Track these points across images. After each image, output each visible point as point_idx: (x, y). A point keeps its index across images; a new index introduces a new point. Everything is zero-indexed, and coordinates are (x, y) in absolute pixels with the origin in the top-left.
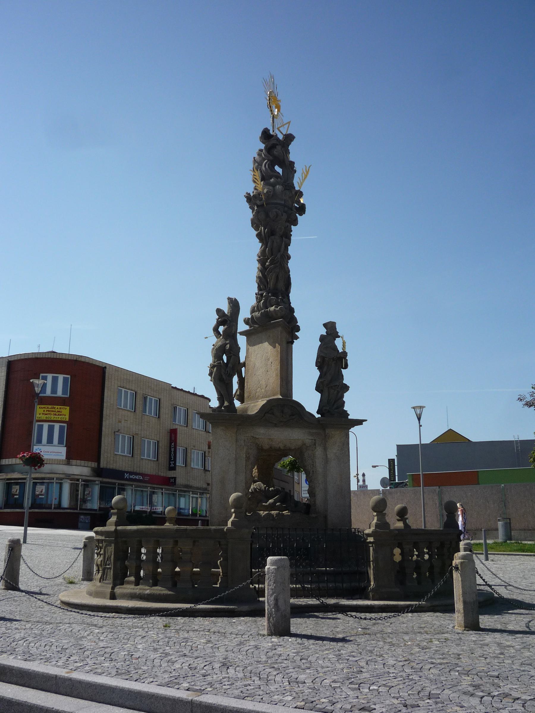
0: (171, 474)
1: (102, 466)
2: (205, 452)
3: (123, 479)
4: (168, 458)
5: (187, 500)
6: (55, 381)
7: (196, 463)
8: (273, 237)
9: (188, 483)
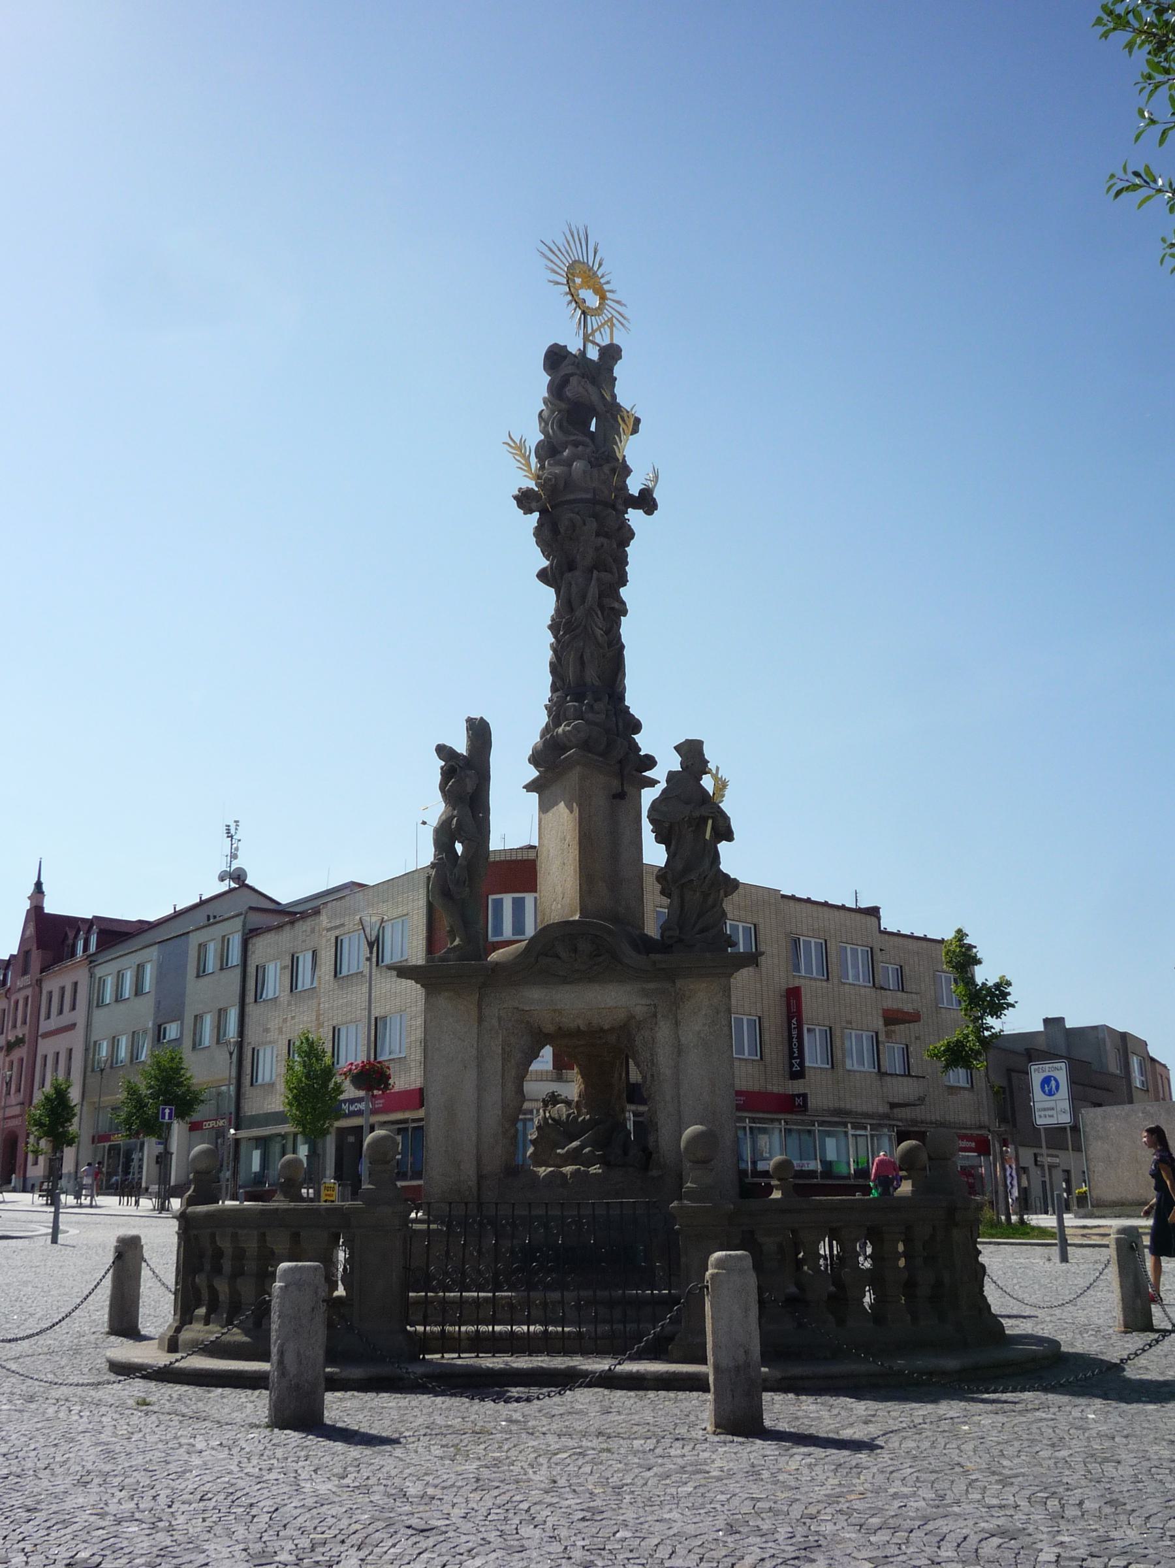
0: (796, 1087)
2: (877, 1033)
4: (786, 1051)
5: (843, 1142)
7: (858, 1061)
8: (568, 575)
9: (843, 1106)
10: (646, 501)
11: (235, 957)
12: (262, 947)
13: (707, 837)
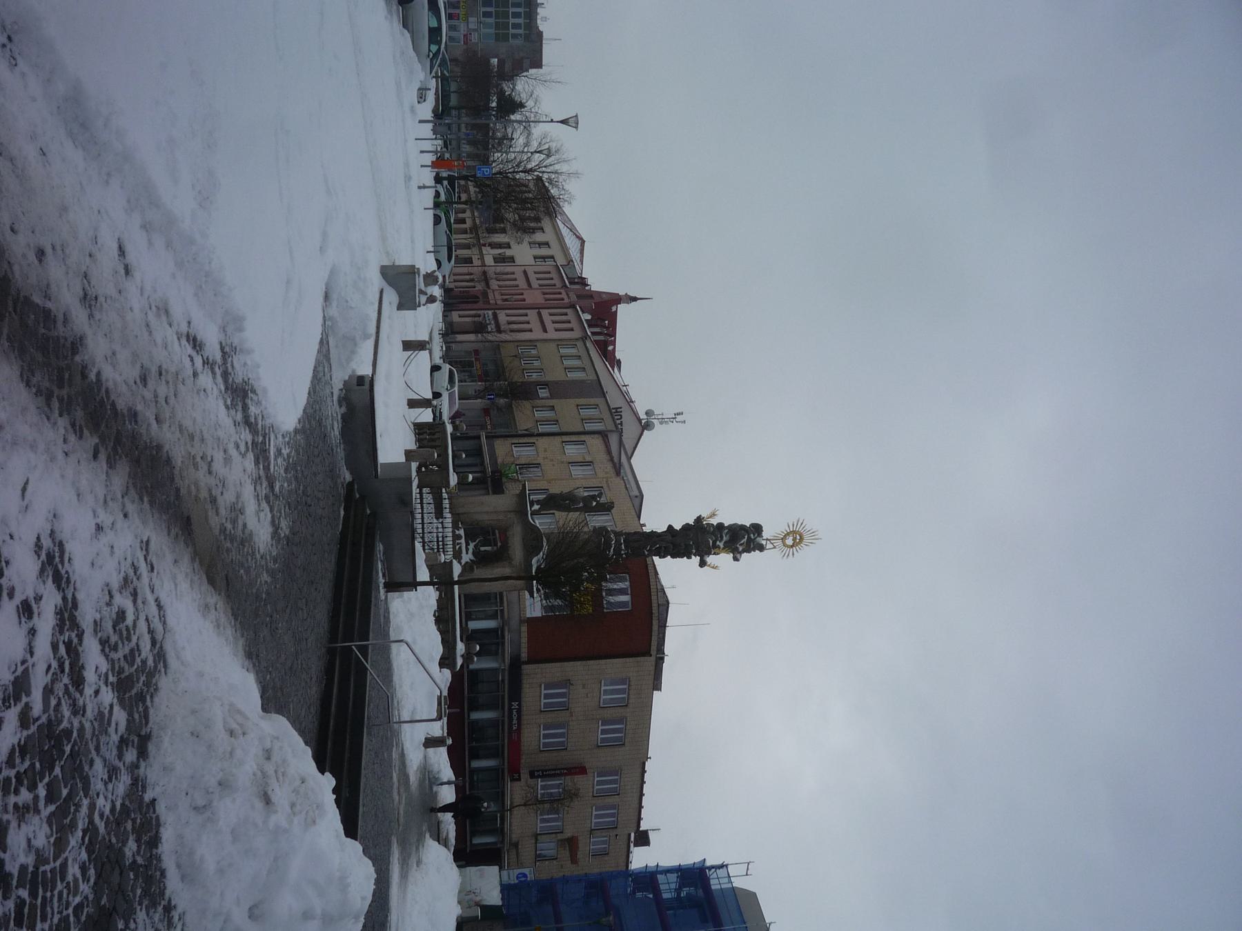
0: (525, 775)
1: (524, 667)
3: (511, 700)
6: (622, 592)
10: (703, 564)
11: (589, 427)
12: (595, 443)
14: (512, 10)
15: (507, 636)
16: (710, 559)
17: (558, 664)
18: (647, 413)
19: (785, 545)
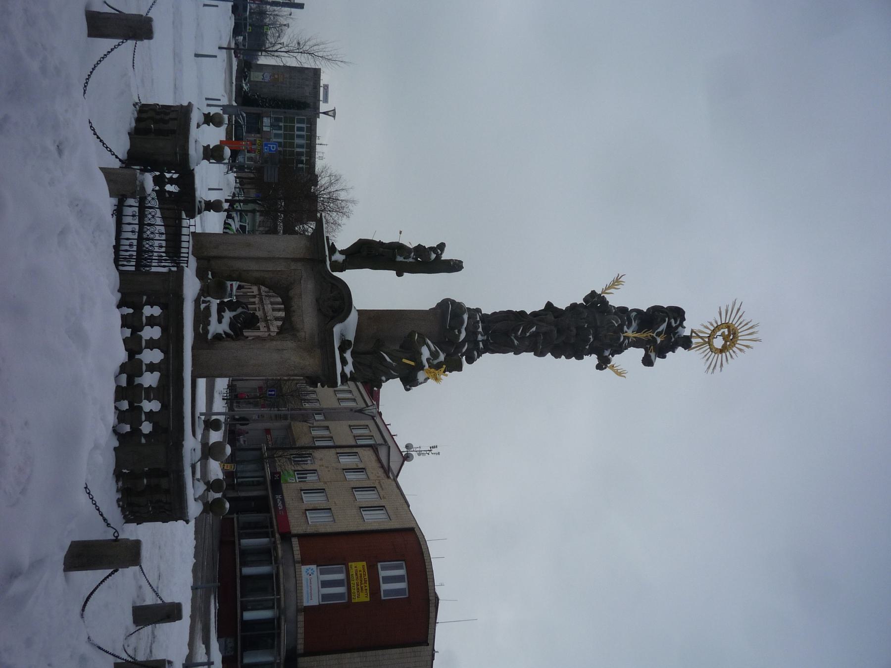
11: (360, 442)
12: (367, 454)
13: (404, 360)
14: (297, 125)
15: (284, 627)
16: (616, 360)
17: (335, 656)
18: (407, 447)
19: (712, 349)
